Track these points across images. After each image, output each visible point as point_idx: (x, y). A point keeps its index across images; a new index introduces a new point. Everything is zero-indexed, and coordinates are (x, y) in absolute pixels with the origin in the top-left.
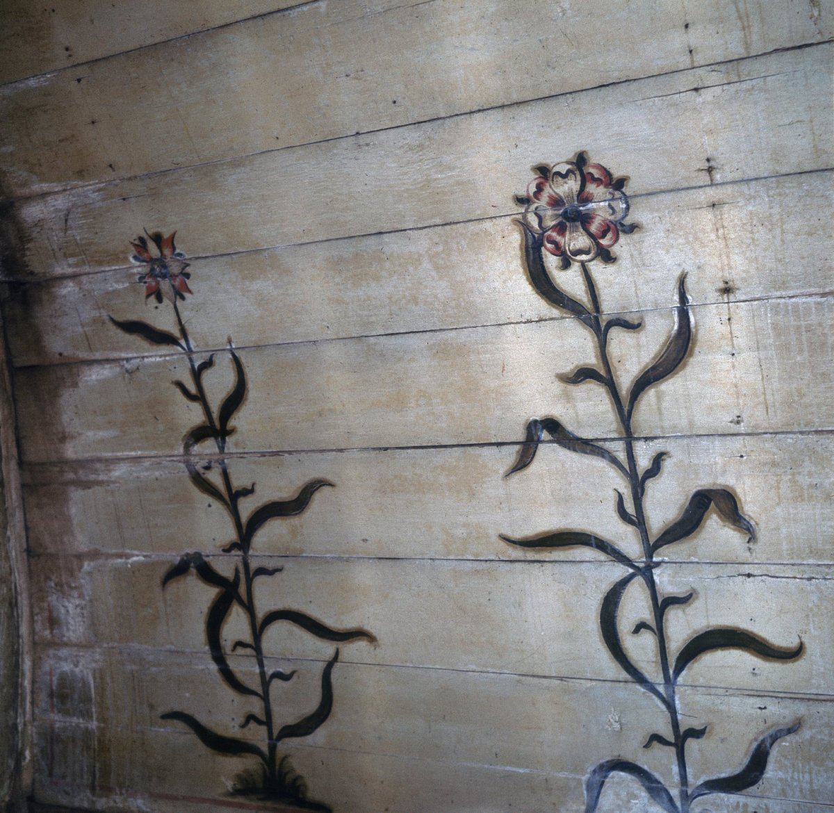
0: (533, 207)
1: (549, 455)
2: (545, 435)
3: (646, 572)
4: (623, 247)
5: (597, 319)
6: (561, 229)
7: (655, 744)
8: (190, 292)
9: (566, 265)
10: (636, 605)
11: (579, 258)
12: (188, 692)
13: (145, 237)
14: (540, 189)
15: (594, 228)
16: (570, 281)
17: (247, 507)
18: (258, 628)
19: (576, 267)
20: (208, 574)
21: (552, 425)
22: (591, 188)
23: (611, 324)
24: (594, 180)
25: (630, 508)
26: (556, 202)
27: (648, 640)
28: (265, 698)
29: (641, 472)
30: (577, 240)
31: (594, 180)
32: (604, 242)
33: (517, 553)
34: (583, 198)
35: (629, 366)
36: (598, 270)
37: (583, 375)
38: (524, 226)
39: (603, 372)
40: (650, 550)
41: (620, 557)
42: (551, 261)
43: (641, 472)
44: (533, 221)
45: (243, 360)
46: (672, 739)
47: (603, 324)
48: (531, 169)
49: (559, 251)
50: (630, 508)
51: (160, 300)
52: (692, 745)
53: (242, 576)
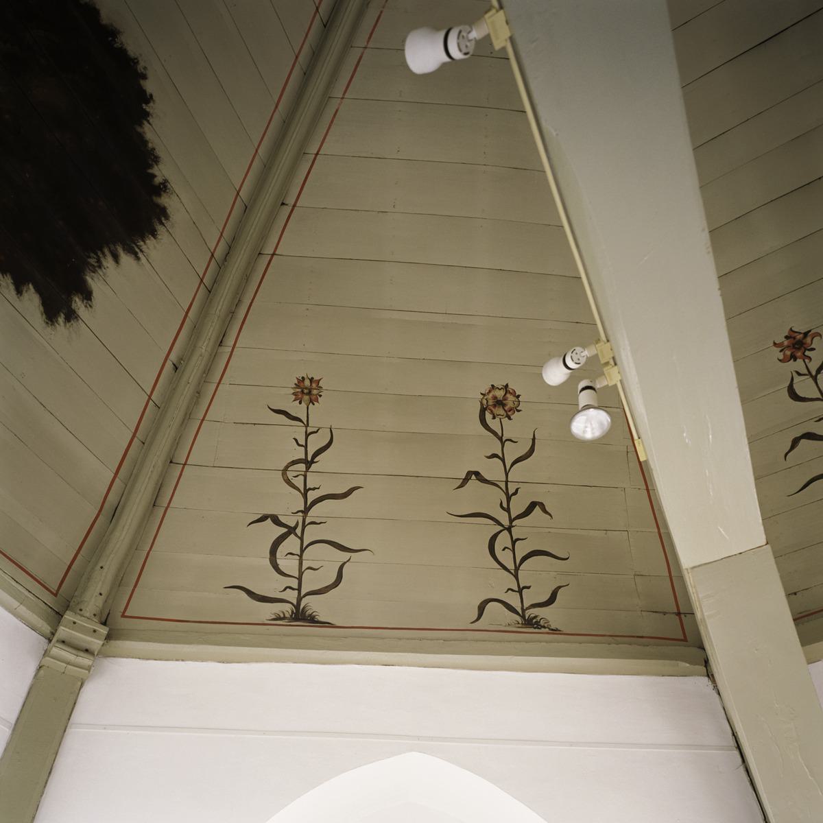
0: (486, 397)
1: (473, 481)
2: (473, 477)
3: (509, 529)
4: (515, 416)
5: (502, 438)
6: (495, 406)
7: (510, 591)
8: (318, 402)
9: (494, 418)
10: (503, 540)
11: (499, 417)
12: (575, 411)
13: (305, 377)
14: (490, 391)
15: (506, 408)
16: (494, 424)
17: (312, 496)
18: (304, 547)
19: (497, 419)
20: (276, 521)
21: (477, 474)
22: (508, 395)
23: (507, 440)
24: (510, 393)
25: (505, 505)
26: (495, 398)
27: (509, 553)
28: (300, 579)
29: (510, 493)
30: (500, 411)
31: (510, 393)
32: (509, 413)
33: (497, 483)
34: (505, 398)
35: (511, 453)
36: (505, 420)
37: (494, 456)
38: (482, 404)
39: (501, 456)
40: (511, 521)
41: (499, 523)
42: (488, 416)
43: (510, 493)
44: (485, 402)
45: (333, 431)
46: (517, 589)
47: (504, 440)
48: (53, 324)
49: (492, 412)
50: (505, 505)
51: (300, 403)
52: (525, 591)
53: (300, 524)
